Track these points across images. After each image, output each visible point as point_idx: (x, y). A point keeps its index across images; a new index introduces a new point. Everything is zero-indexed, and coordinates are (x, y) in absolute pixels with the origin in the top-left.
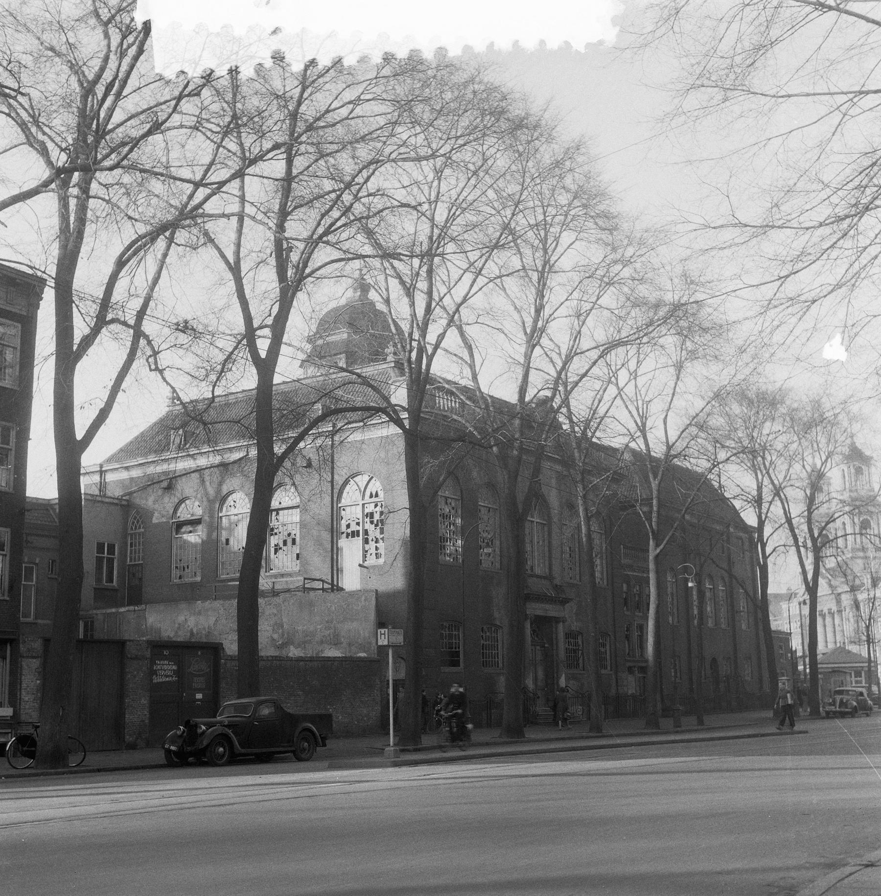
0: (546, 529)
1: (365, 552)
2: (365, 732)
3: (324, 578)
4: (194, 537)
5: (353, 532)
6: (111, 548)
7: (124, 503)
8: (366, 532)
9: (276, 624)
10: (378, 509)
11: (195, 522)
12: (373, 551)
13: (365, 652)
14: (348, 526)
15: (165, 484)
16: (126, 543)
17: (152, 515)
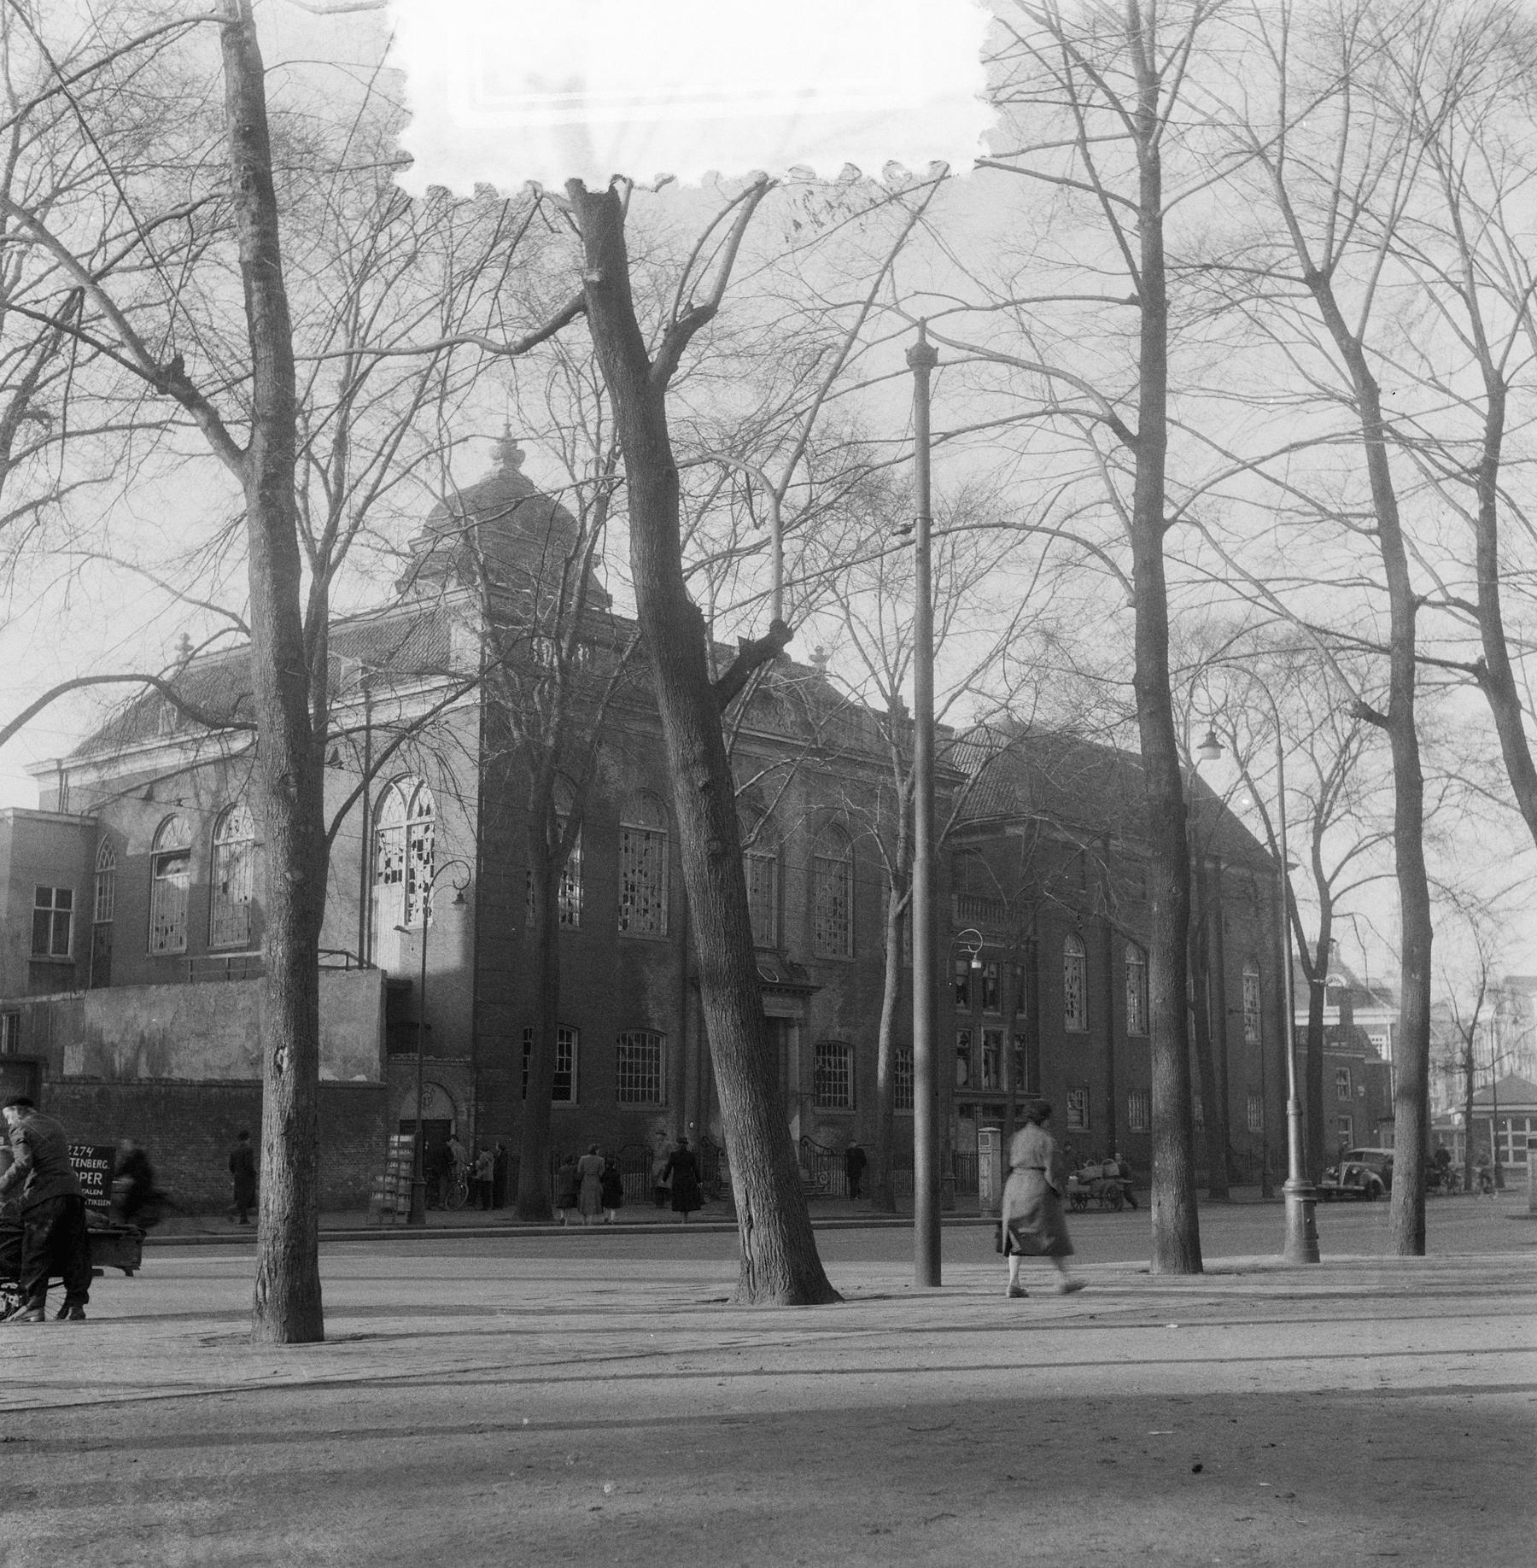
0: (775, 868)
1: (409, 906)
2: (213, 1207)
3: (349, 949)
4: (180, 879)
5: (394, 873)
6: (64, 897)
7: (89, 822)
8: (412, 873)
9: (251, 1024)
10: (430, 834)
11: (184, 855)
12: (420, 905)
13: (364, 1072)
14: (388, 863)
15: (143, 793)
16: (93, 886)
17: (125, 845)
